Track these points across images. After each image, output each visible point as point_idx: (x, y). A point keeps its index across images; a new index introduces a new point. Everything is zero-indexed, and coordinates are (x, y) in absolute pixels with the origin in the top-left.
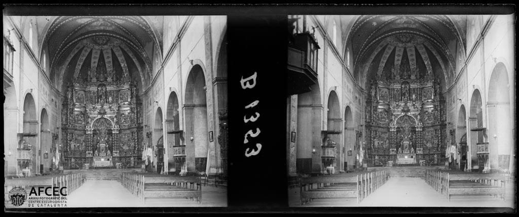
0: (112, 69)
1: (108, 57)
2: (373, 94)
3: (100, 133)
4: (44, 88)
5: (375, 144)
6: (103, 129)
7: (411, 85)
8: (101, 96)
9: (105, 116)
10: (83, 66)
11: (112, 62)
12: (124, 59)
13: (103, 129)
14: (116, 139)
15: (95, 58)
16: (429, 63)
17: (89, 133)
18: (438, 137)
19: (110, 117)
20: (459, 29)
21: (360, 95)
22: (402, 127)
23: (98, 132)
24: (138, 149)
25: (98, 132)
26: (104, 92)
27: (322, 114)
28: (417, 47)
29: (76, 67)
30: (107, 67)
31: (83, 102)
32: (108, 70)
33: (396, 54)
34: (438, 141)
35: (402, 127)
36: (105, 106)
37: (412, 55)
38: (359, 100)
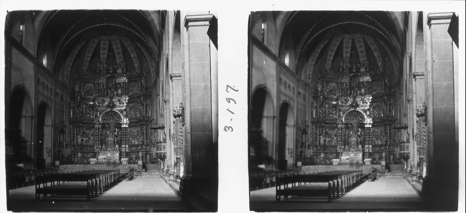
0: (122, 60)
1: (117, 48)
2: (320, 89)
3: (353, 128)
4: (285, 82)
5: (321, 141)
6: (355, 122)
7: (117, 80)
8: (353, 88)
9: (115, 110)
10: (335, 57)
11: (121, 53)
12: (133, 49)
13: (355, 122)
14: (125, 134)
15: (347, 47)
16: (379, 54)
17: (124, 126)
18: (143, 133)
19: (363, 110)
20: (150, 21)
21: (305, 91)
22: (108, 124)
23: (350, 126)
24: (146, 143)
25: (350, 126)
26: (357, 83)
27: (155, 108)
28: (101, 42)
29: (328, 58)
30: (117, 57)
31: (93, 95)
32: (361, 59)
33: (101, 48)
34: (387, 138)
35: (108, 124)
36: (357, 99)
37: (361, 47)
38: (304, 95)
